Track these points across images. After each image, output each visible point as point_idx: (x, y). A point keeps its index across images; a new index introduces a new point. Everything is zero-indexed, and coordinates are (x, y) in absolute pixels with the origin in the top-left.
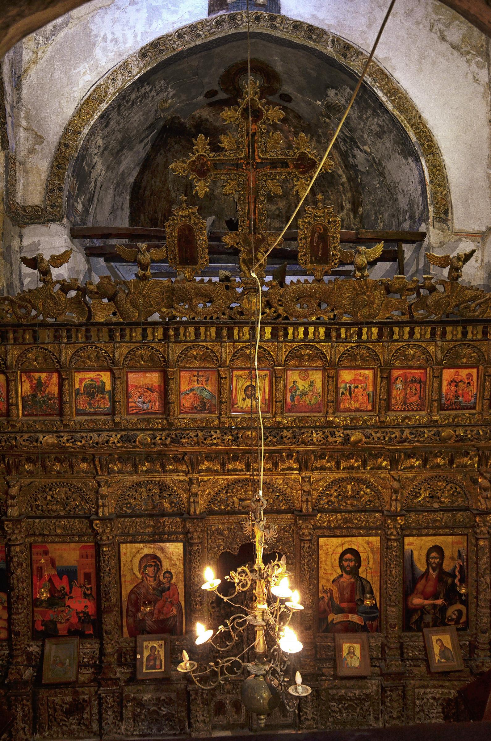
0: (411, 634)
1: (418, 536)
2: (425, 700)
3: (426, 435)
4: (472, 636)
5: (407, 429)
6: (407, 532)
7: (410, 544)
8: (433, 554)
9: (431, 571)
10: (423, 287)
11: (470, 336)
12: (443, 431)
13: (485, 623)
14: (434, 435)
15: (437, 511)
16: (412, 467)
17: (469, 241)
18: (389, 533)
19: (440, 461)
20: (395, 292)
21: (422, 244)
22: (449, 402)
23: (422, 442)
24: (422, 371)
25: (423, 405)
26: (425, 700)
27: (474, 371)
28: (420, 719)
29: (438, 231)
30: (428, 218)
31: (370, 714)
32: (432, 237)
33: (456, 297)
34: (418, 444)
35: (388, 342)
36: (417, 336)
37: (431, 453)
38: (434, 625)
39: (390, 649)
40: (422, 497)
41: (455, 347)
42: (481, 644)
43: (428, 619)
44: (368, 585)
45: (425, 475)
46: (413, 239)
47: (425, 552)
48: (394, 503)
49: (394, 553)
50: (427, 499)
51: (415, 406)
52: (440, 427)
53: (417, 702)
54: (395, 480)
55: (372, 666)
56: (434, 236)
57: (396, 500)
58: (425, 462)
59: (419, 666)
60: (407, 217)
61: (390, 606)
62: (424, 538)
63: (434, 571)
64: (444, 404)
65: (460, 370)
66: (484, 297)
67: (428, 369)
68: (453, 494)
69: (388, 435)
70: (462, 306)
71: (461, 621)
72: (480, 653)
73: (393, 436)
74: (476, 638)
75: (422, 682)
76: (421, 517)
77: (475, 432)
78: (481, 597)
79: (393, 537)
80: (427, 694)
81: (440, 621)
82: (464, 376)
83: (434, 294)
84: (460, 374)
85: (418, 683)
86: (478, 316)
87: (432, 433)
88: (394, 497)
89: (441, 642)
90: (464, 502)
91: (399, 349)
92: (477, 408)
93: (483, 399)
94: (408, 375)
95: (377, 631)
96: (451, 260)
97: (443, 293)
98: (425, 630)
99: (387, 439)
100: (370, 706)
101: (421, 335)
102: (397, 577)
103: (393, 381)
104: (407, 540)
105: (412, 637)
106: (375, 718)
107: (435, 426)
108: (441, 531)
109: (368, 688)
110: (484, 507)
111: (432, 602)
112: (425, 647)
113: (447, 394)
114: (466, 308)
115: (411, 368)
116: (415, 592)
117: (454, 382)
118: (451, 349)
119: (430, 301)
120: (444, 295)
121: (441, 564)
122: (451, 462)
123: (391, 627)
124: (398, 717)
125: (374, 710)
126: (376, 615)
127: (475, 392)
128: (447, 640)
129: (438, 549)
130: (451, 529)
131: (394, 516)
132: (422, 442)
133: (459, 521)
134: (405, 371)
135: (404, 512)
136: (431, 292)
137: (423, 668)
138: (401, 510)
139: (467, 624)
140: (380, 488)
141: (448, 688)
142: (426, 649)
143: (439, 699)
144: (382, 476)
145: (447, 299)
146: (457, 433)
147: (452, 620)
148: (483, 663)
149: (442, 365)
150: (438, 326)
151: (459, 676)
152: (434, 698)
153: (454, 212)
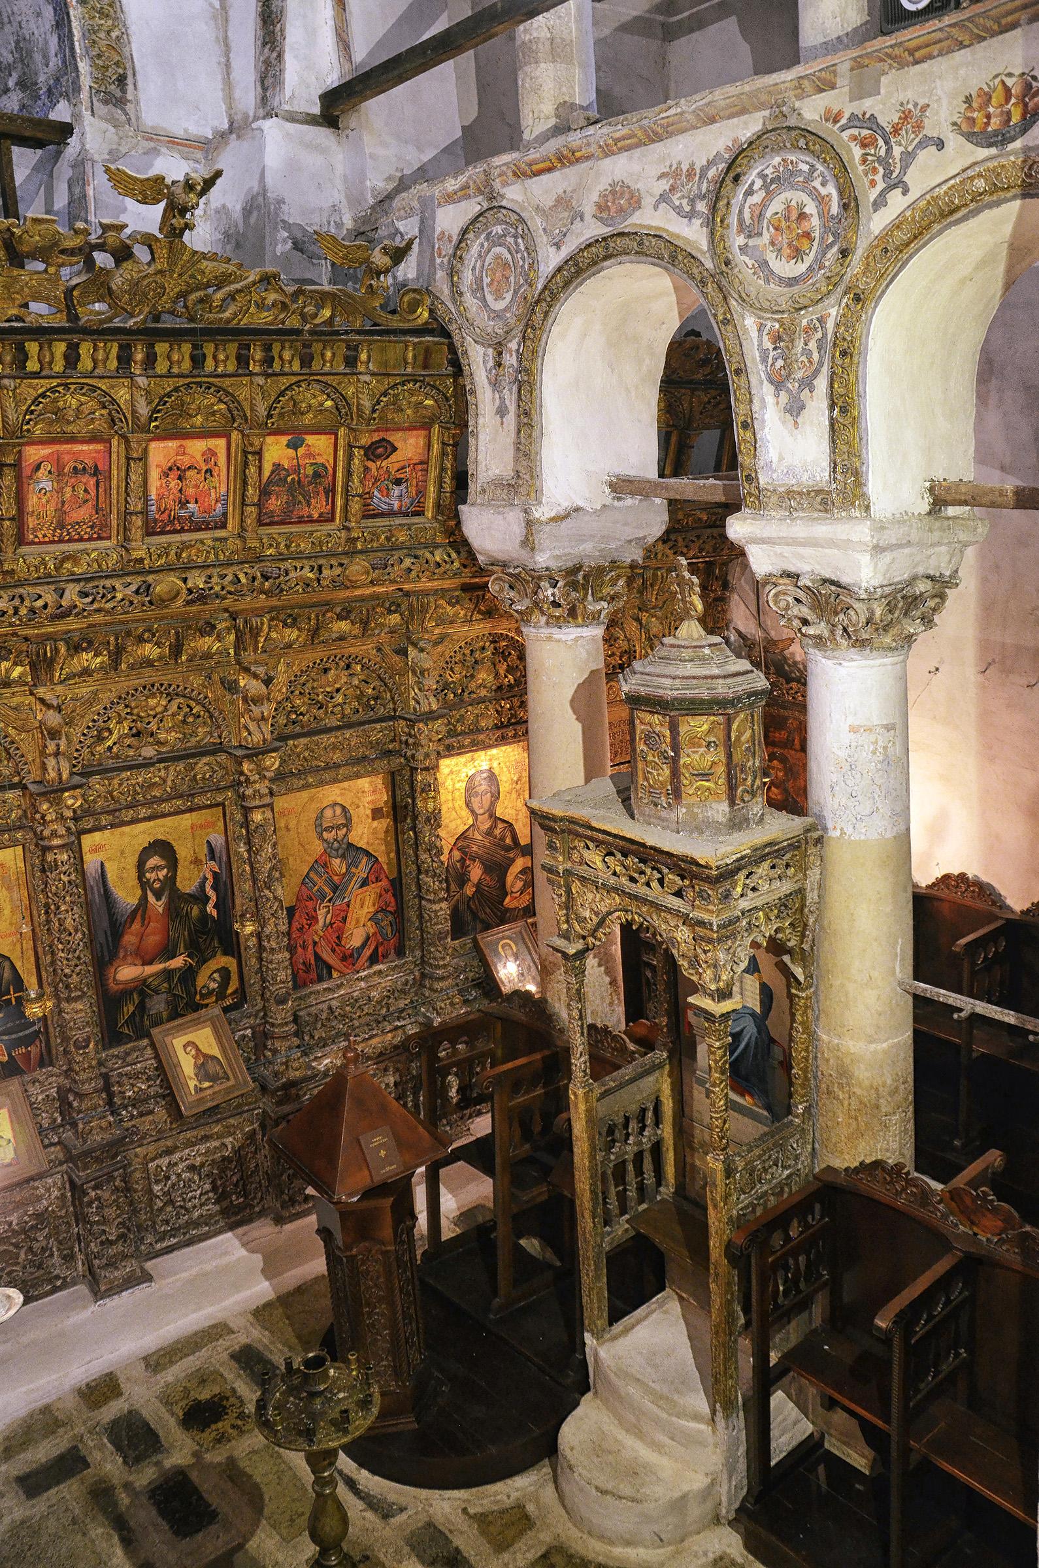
0: (122, 1049)
1: (113, 826)
2: (173, 1177)
3: (119, 596)
4: (256, 1016)
5: (71, 586)
6: (89, 823)
7: (96, 849)
8: (154, 861)
9: (151, 898)
10: (101, 247)
11: (209, 364)
12: (158, 582)
13: (282, 982)
14: (137, 592)
15: (153, 764)
16: (86, 672)
17: (178, 156)
18: (46, 833)
19: (149, 650)
20: (33, 256)
21: (59, 153)
22: (165, 516)
23: (107, 612)
24: (99, 447)
25: (105, 525)
26: (173, 1177)
27: (222, 442)
28: (167, 1222)
29: (104, 125)
30: (77, 89)
31: (51, 1255)
32: (88, 136)
33: (180, 275)
34: (98, 618)
35: (14, 378)
36: (86, 364)
37: (129, 634)
38: (171, 1018)
39: (80, 1096)
40: (115, 737)
41: (176, 389)
42: (281, 1025)
43: (158, 1005)
44: (7, 964)
45: (118, 686)
46: (39, 135)
47: (132, 860)
48: (51, 762)
49: (65, 878)
50: (128, 741)
51: (85, 531)
52: (150, 572)
53: (156, 1188)
54: (49, 706)
55: (45, 1147)
56: (94, 135)
57: (57, 754)
58: (117, 655)
59: (151, 1112)
60: (11, 84)
61: (69, 1000)
62: (126, 829)
63: (158, 899)
64: (155, 521)
65: (188, 443)
66: (242, 278)
67: (115, 442)
68: (184, 722)
69: (27, 603)
70: (193, 297)
71: (229, 991)
72: (277, 1045)
73: (40, 603)
74: (265, 1014)
75: (162, 1143)
76: (116, 782)
77: (230, 578)
78: (268, 929)
79: (56, 842)
80: (176, 1164)
81: (185, 1003)
82: (199, 457)
83: (127, 265)
84: (188, 451)
85: (152, 1149)
86: (229, 321)
87: (134, 588)
88: (51, 748)
89: (192, 1048)
90: (211, 733)
91: (43, 395)
92: (230, 526)
93: (243, 503)
94: (66, 457)
95: (42, 1064)
96: (168, 187)
97: (149, 264)
98: (155, 1031)
99: (23, 611)
100: (47, 1238)
101: (95, 361)
102: (76, 931)
103: (27, 472)
104: (87, 841)
105: (128, 1054)
106: (64, 1258)
107: (138, 573)
108: (166, 807)
109: (39, 1199)
110: (257, 738)
111: (162, 966)
112: (160, 1068)
113: (161, 497)
114: (201, 301)
115: (73, 440)
116: (121, 955)
117: (177, 471)
118: (169, 395)
119: (118, 282)
120: (151, 270)
121: (171, 880)
122: (177, 650)
123: (78, 1048)
124: (122, 1237)
125: (60, 1243)
126: (36, 1027)
127: (223, 490)
128: (205, 1038)
129: (162, 848)
130: (188, 798)
131: (54, 792)
132: (107, 612)
133: (203, 778)
134: (57, 447)
135: (77, 779)
136: (118, 262)
137: (161, 1113)
138: (72, 774)
139: (242, 994)
140: (11, 731)
141: (219, 1136)
142: (164, 1072)
143: (202, 1165)
144: (15, 701)
145: (159, 278)
146: (190, 585)
147: (210, 993)
148: (286, 1063)
149: (148, 431)
150: (137, 340)
151: (239, 1105)
152: (192, 1168)
153: (140, 84)
